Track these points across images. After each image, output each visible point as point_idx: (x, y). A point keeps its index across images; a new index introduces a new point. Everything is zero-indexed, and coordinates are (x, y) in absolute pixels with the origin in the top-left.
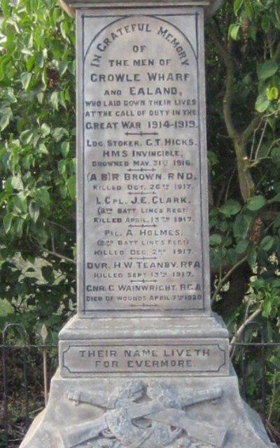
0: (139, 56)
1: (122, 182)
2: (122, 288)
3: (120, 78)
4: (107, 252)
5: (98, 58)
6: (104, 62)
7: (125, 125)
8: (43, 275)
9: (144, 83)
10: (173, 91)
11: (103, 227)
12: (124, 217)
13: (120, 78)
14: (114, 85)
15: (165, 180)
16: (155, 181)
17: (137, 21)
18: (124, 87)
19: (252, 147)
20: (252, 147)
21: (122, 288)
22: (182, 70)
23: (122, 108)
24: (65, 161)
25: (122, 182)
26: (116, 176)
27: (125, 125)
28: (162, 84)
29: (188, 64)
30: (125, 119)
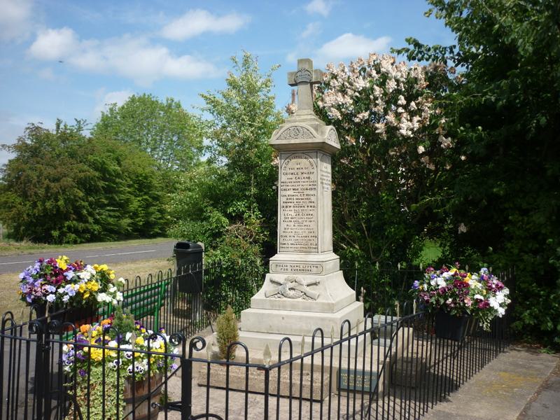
0: (298, 166)
1: (292, 208)
2: (292, 244)
3: (292, 174)
4: (407, 62)
5: (285, 167)
6: (287, 169)
7: (294, 189)
8: (36, 243)
9: (300, 175)
10: (309, 178)
11: (286, 213)
12: (293, 220)
13: (292, 174)
14: (290, 176)
15: (306, 208)
16: (303, 208)
17: (297, 155)
18: (293, 176)
19: (112, 208)
20: (112, 208)
21: (292, 244)
22: (312, 171)
23: (293, 184)
24: (367, 329)
25: (292, 208)
26: (290, 207)
27: (294, 189)
28: (305, 176)
29: (391, 48)
30: (294, 187)
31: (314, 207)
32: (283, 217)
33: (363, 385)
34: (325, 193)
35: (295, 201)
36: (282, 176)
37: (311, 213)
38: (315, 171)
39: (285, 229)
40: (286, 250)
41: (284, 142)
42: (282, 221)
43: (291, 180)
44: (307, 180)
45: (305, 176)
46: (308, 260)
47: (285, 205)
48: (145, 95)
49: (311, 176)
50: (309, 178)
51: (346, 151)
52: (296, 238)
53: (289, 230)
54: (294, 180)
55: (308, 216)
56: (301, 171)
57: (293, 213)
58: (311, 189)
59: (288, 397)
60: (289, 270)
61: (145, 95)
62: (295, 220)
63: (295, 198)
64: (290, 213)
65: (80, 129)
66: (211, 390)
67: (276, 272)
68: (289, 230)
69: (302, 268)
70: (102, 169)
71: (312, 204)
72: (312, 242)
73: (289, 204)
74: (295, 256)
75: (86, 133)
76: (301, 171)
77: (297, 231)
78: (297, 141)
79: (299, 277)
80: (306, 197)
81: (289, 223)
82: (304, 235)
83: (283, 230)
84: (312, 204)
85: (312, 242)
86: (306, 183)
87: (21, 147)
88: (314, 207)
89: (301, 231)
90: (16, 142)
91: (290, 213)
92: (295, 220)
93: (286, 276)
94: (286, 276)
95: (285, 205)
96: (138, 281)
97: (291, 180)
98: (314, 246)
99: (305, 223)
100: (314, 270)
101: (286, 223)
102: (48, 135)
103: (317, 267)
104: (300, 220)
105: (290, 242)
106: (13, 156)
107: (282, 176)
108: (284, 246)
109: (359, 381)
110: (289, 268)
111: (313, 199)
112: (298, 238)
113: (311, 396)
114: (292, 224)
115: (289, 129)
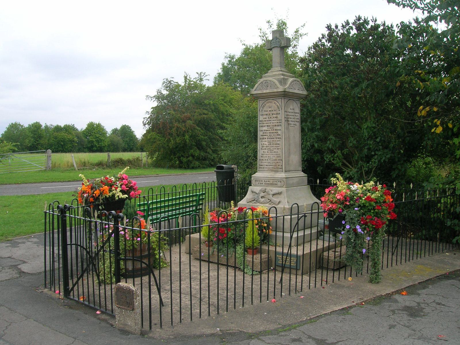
0: (270, 109)
1: (266, 140)
3: (266, 115)
6: (263, 111)
9: (271, 116)
10: (277, 117)
12: (267, 148)
13: (266, 115)
14: (265, 116)
26: (265, 138)
28: (274, 116)
31: (280, 138)
32: (261, 146)
33: (290, 264)
34: (290, 128)
35: (268, 134)
36: (260, 116)
37: (278, 142)
38: (280, 112)
39: (262, 154)
40: (262, 169)
41: (259, 92)
42: (260, 149)
43: (265, 120)
44: (275, 119)
45: (274, 116)
46: (276, 177)
47: (262, 137)
48: (313, 44)
49: (278, 116)
50: (277, 117)
51: (306, 97)
52: (269, 161)
53: (265, 155)
54: (267, 119)
55: (276, 145)
56: (272, 112)
57: (266, 143)
58: (278, 126)
59: (234, 267)
60: (264, 184)
61: (313, 44)
62: (268, 148)
63: (268, 132)
64: (265, 143)
65: (201, 80)
66: (291, 269)
67: (255, 185)
68: (265, 155)
69: (271, 183)
70: (216, 110)
71: (279, 137)
72: (279, 164)
73: (265, 137)
74: (296, 174)
75: (209, 83)
76: (272, 112)
77: (269, 156)
78: (268, 91)
79: (268, 189)
80: (275, 131)
81: (265, 150)
82: (274, 158)
83: (261, 155)
84: (279, 137)
85: (279, 164)
86: (275, 121)
87: (159, 97)
88: (280, 138)
89: (272, 156)
90: (156, 94)
91: (265, 143)
92: (268, 148)
93: (260, 188)
94: (260, 188)
95: (262, 137)
96: (185, 188)
97: (265, 120)
98: (280, 167)
99: (275, 150)
100: (279, 183)
101: (263, 150)
102: (178, 86)
103: (281, 182)
104: (271, 148)
105: (265, 164)
106: (155, 104)
107: (260, 116)
108: (262, 167)
109: (288, 261)
110: (263, 182)
111: (279, 132)
112: (270, 161)
113: (235, 265)
114: (266, 151)
115: (262, 83)
